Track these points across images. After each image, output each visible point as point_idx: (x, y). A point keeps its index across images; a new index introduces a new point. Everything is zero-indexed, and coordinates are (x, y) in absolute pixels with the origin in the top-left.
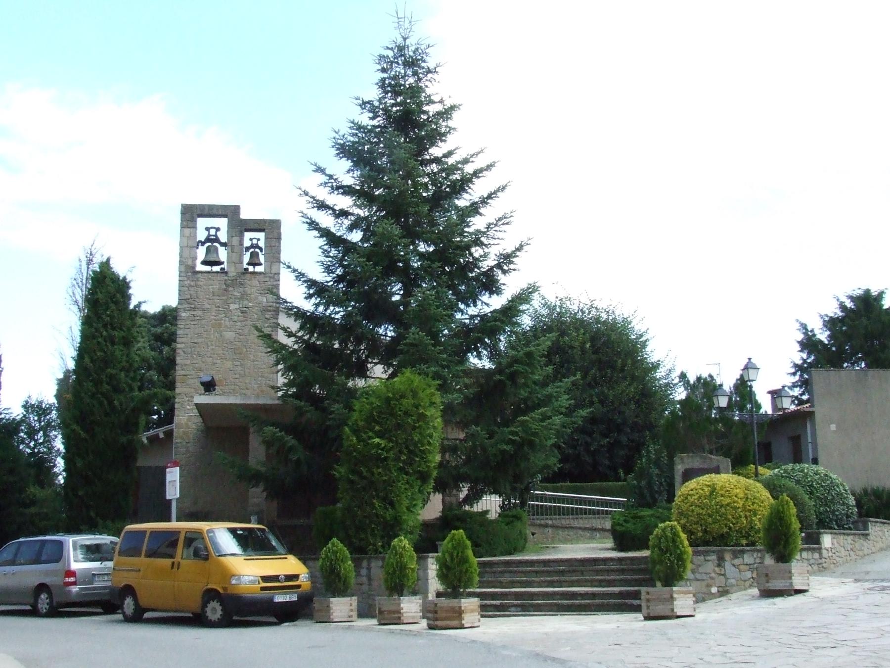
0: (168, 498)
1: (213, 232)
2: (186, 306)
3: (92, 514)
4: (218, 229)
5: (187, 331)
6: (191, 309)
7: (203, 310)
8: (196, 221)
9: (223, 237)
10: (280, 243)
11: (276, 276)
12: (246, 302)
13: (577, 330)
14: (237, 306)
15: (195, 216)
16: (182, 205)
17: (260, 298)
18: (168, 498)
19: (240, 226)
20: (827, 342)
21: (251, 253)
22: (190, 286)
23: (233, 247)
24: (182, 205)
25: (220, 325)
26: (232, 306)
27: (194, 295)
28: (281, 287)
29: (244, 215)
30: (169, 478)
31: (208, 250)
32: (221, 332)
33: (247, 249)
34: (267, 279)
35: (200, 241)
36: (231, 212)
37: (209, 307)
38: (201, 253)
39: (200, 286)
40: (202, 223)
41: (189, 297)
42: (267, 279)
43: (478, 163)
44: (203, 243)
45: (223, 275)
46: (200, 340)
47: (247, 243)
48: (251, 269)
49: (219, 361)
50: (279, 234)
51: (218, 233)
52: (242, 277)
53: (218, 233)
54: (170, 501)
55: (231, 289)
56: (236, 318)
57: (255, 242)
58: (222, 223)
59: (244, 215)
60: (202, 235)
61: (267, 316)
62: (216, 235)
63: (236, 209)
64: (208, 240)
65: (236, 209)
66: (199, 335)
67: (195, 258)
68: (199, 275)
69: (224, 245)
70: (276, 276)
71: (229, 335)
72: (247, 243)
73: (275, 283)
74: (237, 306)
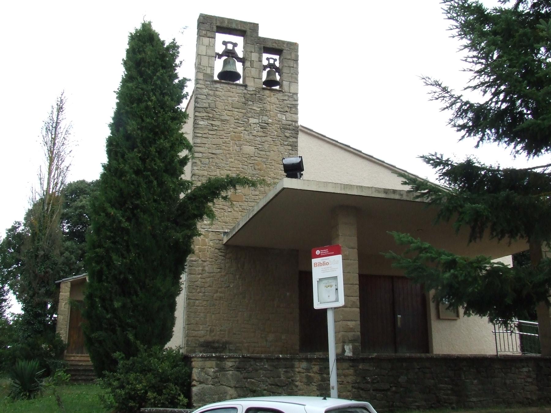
2: (205, 114)
3: (131, 337)
4: (235, 45)
5: (204, 141)
6: (209, 118)
7: (222, 120)
8: (260, 37)
10: (297, 64)
11: (295, 96)
12: (265, 118)
13: (198, 208)
14: (256, 121)
16: (258, 24)
17: (279, 115)
20: (166, 346)
22: (209, 95)
24: (258, 24)
26: (252, 121)
27: (213, 105)
28: (299, 107)
31: (226, 63)
32: (240, 146)
33: (265, 67)
34: (286, 98)
35: (218, 54)
37: (228, 118)
39: (219, 97)
40: (221, 40)
41: (207, 105)
44: (220, 56)
45: (243, 88)
46: (218, 151)
47: (265, 62)
50: (297, 56)
51: (235, 48)
52: (261, 93)
53: (235, 48)
56: (255, 133)
59: (262, 33)
60: (220, 49)
61: (288, 135)
63: (255, 27)
65: (255, 27)
66: (218, 146)
69: (239, 60)
70: (295, 96)
71: (249, 149)
73: (294, 103)
74: (256, 121)
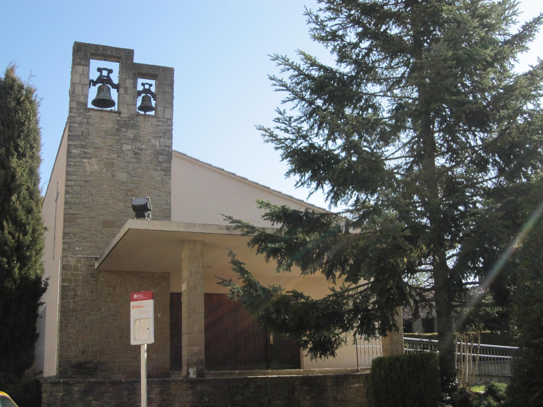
0: (133, 342)
1: (105, 73)
4: (110, 71)
6: (82, 146)
9: (115, 78)
14: (129, 147)
15: (89, 55)
16: (76, 43)
18: (133, 342)
19: (133, 69)
21: (143, 98)
23: (126, 89)
24: (76, 43)
25: (112, 165)
26: (126, 147)
29: (138, 59)
30: (134, 314)
31: (100, 90)
34: (160, 123)
35: (92, 81)
36: (123, 56)
38: (93, 93)
42: (160, 123)
43: (276, 70)
44: (95, 83)
47: (140, 88)
48: (142, 112)
49: (111, 202)
54: (138, 347)
55: (124, 130)
57: (147, 87)
58: (115, 66)
59: (138, 59)
60: (94, 75)
61: (161, 160)
62: (108, 77)
63: (130, 53)
64: (100, 80)
65: (130, 53)
67: (86, 96)
68: (91, 113)
70: (169, 122)
71: (122, 176)
72: (140, 88)
74: (129, 147)
